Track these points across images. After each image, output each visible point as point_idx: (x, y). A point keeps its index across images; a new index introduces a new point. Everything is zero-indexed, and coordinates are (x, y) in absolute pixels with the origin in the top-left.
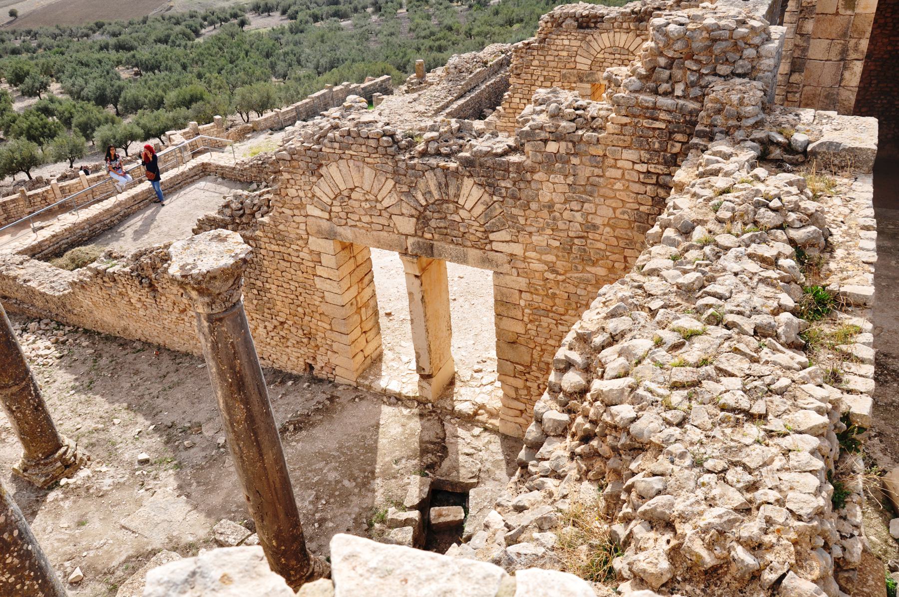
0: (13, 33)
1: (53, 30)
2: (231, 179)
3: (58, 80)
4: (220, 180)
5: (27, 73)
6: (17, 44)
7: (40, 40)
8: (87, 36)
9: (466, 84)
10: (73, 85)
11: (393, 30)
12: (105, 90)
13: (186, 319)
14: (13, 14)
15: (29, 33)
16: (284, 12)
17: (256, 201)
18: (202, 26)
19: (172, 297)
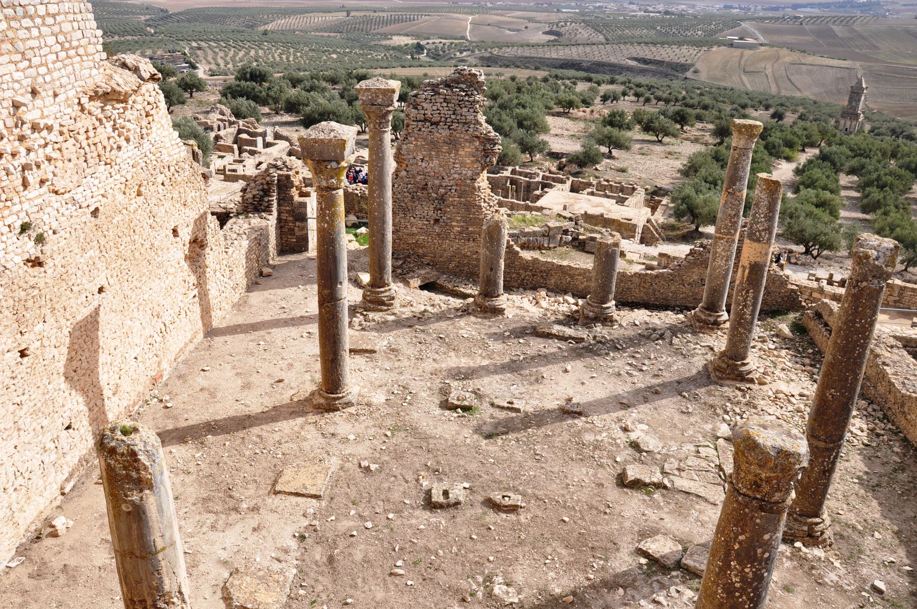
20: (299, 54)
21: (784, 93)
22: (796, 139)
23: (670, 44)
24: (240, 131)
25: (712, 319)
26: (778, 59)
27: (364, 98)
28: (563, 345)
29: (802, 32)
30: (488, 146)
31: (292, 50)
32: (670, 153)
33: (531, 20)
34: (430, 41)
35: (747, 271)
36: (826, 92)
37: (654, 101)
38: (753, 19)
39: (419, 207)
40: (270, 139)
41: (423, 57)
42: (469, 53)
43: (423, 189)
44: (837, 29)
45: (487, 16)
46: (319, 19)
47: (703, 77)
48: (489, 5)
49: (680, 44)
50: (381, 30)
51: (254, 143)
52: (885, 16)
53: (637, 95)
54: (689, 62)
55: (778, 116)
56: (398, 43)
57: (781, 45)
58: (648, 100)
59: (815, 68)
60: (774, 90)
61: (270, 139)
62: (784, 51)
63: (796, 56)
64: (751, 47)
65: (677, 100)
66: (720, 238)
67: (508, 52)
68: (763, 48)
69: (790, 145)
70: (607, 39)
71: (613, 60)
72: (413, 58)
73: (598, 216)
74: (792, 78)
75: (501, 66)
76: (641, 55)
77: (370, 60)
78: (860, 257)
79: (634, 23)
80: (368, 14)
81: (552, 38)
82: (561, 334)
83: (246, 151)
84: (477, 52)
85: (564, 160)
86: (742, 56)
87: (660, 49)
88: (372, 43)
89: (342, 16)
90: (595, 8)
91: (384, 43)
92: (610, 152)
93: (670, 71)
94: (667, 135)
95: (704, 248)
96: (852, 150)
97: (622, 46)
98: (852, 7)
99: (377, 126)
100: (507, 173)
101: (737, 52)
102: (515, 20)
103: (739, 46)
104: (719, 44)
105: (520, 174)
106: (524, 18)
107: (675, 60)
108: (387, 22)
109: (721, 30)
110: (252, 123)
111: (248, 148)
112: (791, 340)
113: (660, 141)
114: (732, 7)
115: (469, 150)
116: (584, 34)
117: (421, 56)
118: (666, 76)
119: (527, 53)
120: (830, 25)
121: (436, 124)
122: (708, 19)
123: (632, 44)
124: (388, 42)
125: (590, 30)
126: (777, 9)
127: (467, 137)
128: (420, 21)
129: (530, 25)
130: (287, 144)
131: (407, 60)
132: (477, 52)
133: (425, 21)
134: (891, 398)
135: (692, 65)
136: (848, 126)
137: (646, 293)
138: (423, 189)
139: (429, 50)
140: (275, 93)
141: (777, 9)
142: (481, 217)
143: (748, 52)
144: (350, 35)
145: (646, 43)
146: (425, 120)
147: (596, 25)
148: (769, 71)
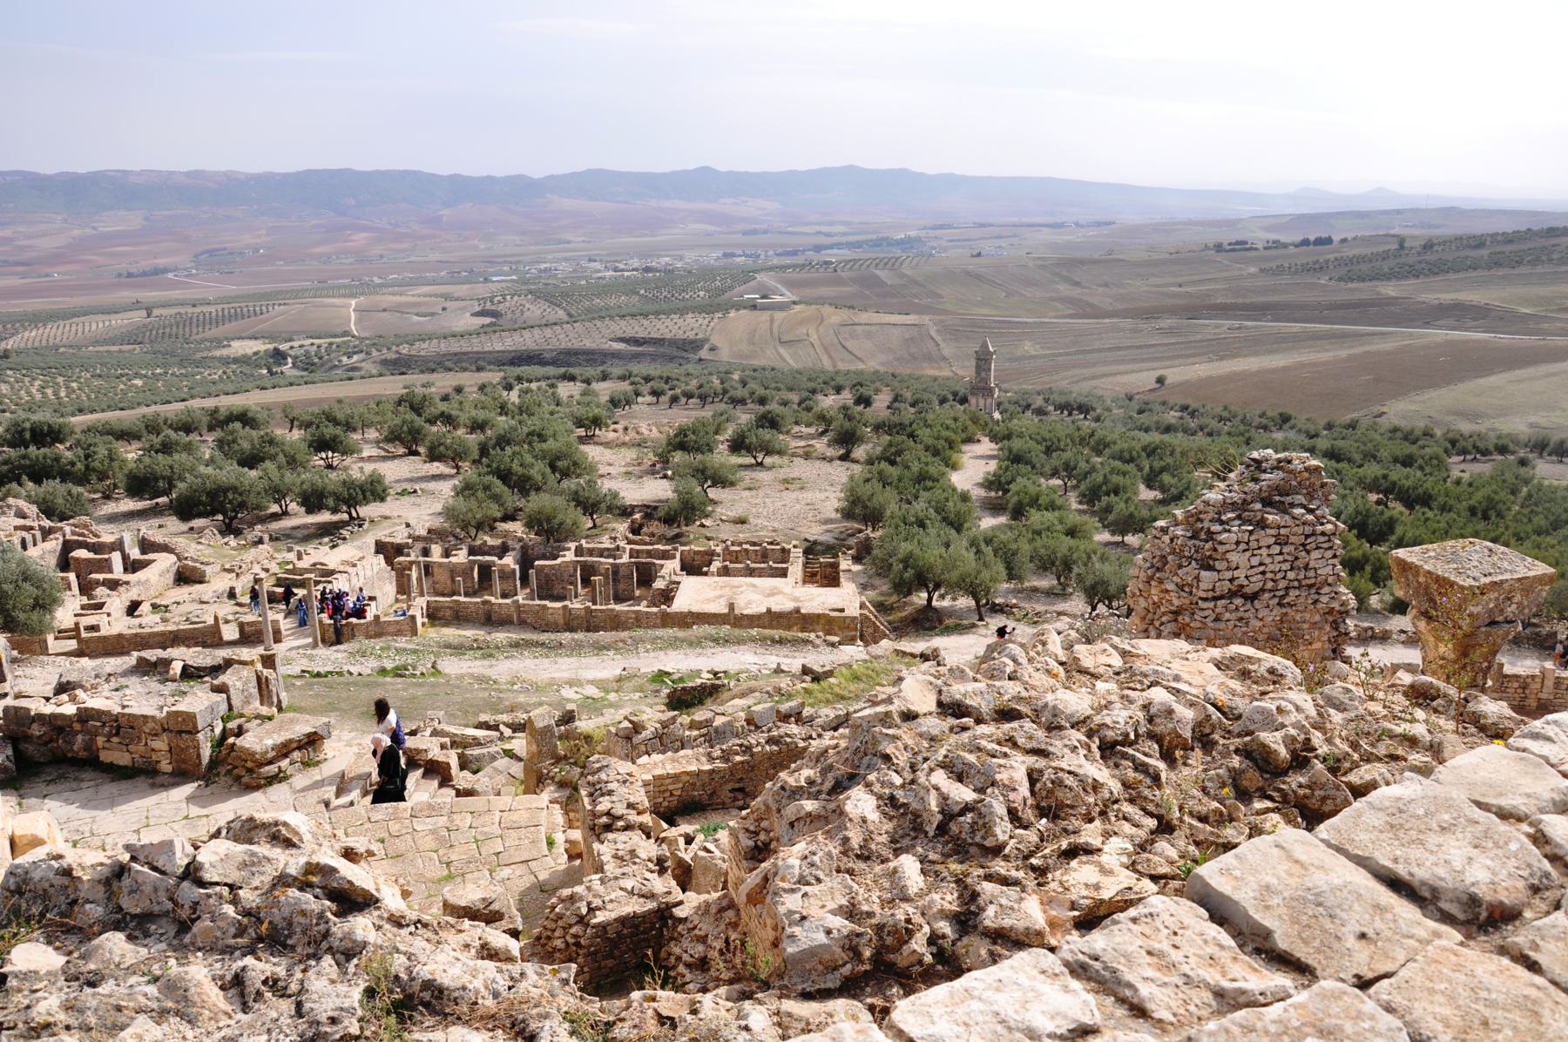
0: (1164, 403)
1: (1219, 410)
6: (1172, 417)
14: (1160, 380)
15: (1184, 408)
20: (74, 385)
21: (842, 366)
22: (953, 436)
23: (668, 313)
24: (68, 546)
27: (1475, 610)
29: (840, 282)
31: (60, 380)
32: (786, 481)
33: (447, 297)
34: (296, 344)
37: (684, 400)
38: (771, 269)
40: (135, 553)
41: (287, 368)
42: (362, 356)
44: (882, 274)
45: (378, 298)
46: (97, 325)
47: (725, 355)
48: (377, 280)
49: (682, 312)
50: (208, 334)
51: (106, 566)
53: (656, 393)
54: (701, 336)
55: (865, 401)
56: (241, 352)
57: (821, 301)
60: (827, 364)
61: (135, 553)
62: (827, 310)
64: (782, 307)
67: (425, 349)
68: (798, 308)
70: (570, 315)
71: (588, 344)
72: (270, 371)
73: (790, 613)
74: (848, 344)
75: (422, 372)
76: (630, 333)
77: (201, 383)
79: (605, 289)
80: (182, 311)
81: (488, 320)
83: (98, 583)
84: (375, 353)
85: (637, 516)
86: (772, 321)
88: (198, 356)
89: (138, 316)
90: (540, 271)
91: (217, 353)
94: (768, 453)
97: (599, 323)
98: (889, 245)
100: (569, 556)
101: (765, 316)
102: (422, 299)
103: (765, 308)
104: (738, 306)
105: (591, 552)
106: (436, 296)
108: (219, 321)
109: (731, 288)
110: (85, 526)
111: (101, 577)
113: (761, 464)
114: (733, 255)
116: (535, 310)
117: (284, 368)
118: (672, 359)
119: (455, 346)
120: (872, 269)
121: (1254, 597)
122: (707, 274)
123: (611, 318)
124: (224, 352)
125: (544, 305)
126: (794, 253)
127: (1317, 618)
128: (272, 313)
129: (448, 304)
130: (173, 558)
131: (262, 377)
132: (375, 353)
133: (280, 315)
135: (706, 340)
139: (295, 358)
140: (102, 462)
141: (794, 253)
143: (779, 315)
144: (157, 347)
145: (633, 316)
146: (1232, 594)
147: (550, 296)
148: (814, 338)
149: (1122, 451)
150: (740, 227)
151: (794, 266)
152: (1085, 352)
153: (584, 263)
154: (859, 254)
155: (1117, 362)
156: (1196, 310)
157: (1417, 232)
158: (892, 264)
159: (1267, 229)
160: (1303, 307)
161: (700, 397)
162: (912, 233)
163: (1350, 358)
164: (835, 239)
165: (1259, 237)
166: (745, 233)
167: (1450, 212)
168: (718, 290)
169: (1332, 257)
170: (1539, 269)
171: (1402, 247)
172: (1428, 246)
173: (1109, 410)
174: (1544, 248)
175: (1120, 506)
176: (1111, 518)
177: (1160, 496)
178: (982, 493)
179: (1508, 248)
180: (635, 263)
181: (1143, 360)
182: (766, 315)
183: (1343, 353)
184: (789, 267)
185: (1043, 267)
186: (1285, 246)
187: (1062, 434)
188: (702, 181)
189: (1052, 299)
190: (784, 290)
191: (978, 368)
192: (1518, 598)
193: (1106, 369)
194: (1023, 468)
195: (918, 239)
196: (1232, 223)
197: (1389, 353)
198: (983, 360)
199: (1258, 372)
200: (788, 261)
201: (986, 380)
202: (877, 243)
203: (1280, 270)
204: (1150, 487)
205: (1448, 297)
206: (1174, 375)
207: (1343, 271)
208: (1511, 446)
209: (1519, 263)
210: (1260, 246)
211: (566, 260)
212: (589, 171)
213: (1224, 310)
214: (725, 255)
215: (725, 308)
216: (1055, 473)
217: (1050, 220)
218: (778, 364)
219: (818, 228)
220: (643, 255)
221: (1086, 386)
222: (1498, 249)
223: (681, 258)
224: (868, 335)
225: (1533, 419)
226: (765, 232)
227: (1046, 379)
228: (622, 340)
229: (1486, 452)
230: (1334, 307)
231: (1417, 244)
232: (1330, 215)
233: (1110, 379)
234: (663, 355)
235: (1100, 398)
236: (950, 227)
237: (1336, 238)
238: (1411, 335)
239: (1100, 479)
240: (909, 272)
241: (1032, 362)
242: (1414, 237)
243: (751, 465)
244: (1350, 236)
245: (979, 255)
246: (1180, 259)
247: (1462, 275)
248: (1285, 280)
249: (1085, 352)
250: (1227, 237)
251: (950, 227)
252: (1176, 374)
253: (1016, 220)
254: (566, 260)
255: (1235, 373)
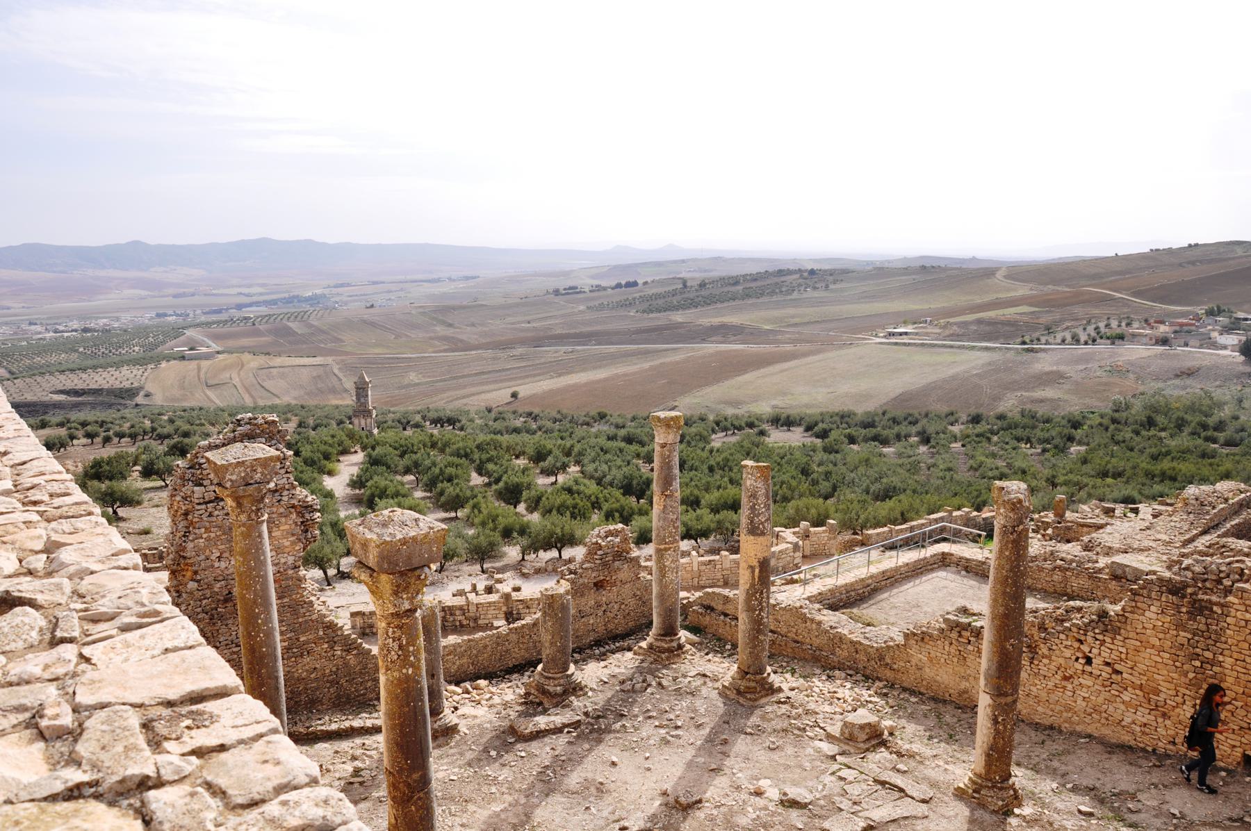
0: (514, 412)
1: (554, 414)
2: (977, 574)
3: (578, 463)
4: (963, 573)
5: (550, 452)
6: (519, 423)
7: (540, 423)
8: (588, 424)
9: (1211, 519)
10: (596, 470)
11: (950, 465)
12: (632, 479)
13: (1070, 687)
14: (514, 395)
15: (530, 414)
16: (808, 429)
17: (1223, 568)
18: (714, 431)
19: (1061, 661)
22: (330, 449)
25: (675, 644)
26: (243, 365)
27: (234, 477)
28: (561, 741)
29: (257, 333)
30: (307, 516)
35: (757, 571)
36: (308, 394)
37: (116, 440)
38: (198, 325)
39: (223, 630)
43: (226, 601)
47: (158, 400)
49: (117, 365)
52: (335, 308)
53: (90, 436)
54: (136, 385)
57: (242, 350)
58: (107, 440)
59: (286, 370)
62: (247, 357)
63: (260, 360)
64: (207, 357)
65: (145, 433)
66: (666, 550)
69: (327, 457)
70: (11, 373)
76: (69, 385)
78: (1013, 504)
82: (552, 726)
86: (199, 369)
87: (93, 375)
92: (115, 512)
93: (113, 400)
95: (575, 573)
96: (395, 449)
97: (39, 379)
99: (253, 515)
101: (193, 365)
104: (168, 358)
107: (117, 385)
109: (163, 342)
112: (700, 644)
114: (166, 315)
115: (287, 527)
118: (110, 406)
120: (284, 321)
123: (51, 374)
126: (219, 312)
127: (282, 510)
134: (862, 657)
135: (141, 388)
136: (363, 425)
137: (527, 650)
138: (226, 601)
141: (219, 312)
142: (314, 617)
145: (72, 370)
148: (236, 381)
149: (458, 449)
150: (171, 291)
151: (218, 322)
152: (455, 378)
153: (25, 326)
154: (275, 310)
155: (482, 384)
156: (540, 340)
157: (697, 275)
158: (300, 317)
159: (592, 277)
160: (617, 333)
161: (130, 436)
162: (318, 292)
163: (651, 368)
164: (255, 299)
165: (586, 283)
166: (175, 296)
167: (717, 260)
168: (152, 345)
169: (637, 295)
170: (775, 298)
171: (685, 286)
172: (702, 285)
173: (472, 420)
174: (777, 284)
175: (450, 490)
176: (443, 499)
177: (487, 480)
178: (348, 491)
179: (753, 285)
180: (75, 325)
181: (501, 381)
182: (194, 364)
183: (646, 365)
184: (214, 323)
185: (423, 314)
186: (605, 289)
187: (415, 441)
188: (132, 254)
189: (431, 338)
190: (210, 343)
191: (358, 395)
192: (259, 470)
193: (474, 390)
194: (382, 469)
195: (324, 296)
196: (566, 274)
197: (677, 363)
198: (361, 390)
199: (586, 384)
200: (214, 318)
201: (366, 404)
202: (289, 301)
203: (601, 307)
204: (480, 474)
205: (716, 321)
206: (525, 390)
207: (646, 305)
208: (756, 423)
209: (762, 295)
210: (587, 290)
211: (6, 324)
212: (24, 245)
213: (560, 339)
214: (158, 315)
215: (157, 360)
216: (407, 471)
217: (431, 277)
218: (205, 404)
219: (240, 290)
220: (82, 317)
221: (458, 404)
222: (748, 285)
223: (118, 319)
224: (283, 376)
225: (774, 402)
226: (193, 295)
227: (428, 401)
228: (62, 392)
229: (740, 428)
230: (640, 331)
231: (695, 283)
232: (637, 265)
233: (476, 397)
234: (102, 403)
235: (468, 412)
236: (349, 285)
237: (640, 282)
238: (693, 349)
239: (437, 471)
240: (315, 323)
241: (409, 389)
242: (693, 279)
243: (161, 487)
244: (649, 280)
245: (372, 306)
246: (528, 303)
247: (726, 304)
248: (606, 313)
249: (455, 378)
250: (562, 284)
251: (349, 285)
252: (526, 390)
253: (402, 278)
254: (6, 324)
255: (570, 386)
